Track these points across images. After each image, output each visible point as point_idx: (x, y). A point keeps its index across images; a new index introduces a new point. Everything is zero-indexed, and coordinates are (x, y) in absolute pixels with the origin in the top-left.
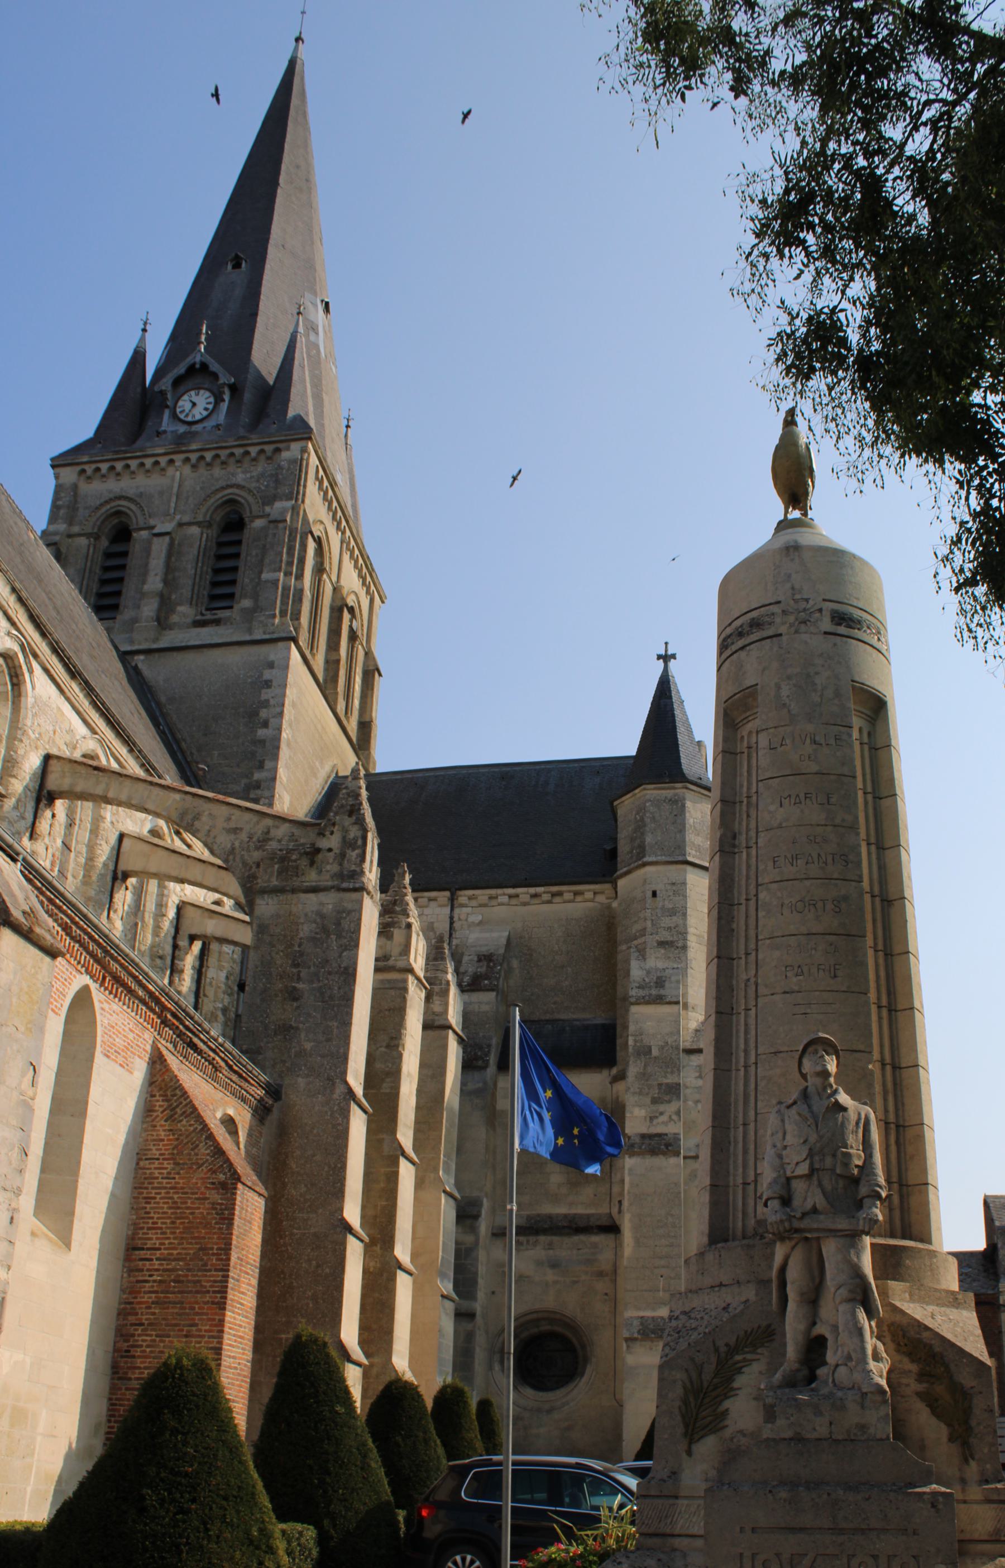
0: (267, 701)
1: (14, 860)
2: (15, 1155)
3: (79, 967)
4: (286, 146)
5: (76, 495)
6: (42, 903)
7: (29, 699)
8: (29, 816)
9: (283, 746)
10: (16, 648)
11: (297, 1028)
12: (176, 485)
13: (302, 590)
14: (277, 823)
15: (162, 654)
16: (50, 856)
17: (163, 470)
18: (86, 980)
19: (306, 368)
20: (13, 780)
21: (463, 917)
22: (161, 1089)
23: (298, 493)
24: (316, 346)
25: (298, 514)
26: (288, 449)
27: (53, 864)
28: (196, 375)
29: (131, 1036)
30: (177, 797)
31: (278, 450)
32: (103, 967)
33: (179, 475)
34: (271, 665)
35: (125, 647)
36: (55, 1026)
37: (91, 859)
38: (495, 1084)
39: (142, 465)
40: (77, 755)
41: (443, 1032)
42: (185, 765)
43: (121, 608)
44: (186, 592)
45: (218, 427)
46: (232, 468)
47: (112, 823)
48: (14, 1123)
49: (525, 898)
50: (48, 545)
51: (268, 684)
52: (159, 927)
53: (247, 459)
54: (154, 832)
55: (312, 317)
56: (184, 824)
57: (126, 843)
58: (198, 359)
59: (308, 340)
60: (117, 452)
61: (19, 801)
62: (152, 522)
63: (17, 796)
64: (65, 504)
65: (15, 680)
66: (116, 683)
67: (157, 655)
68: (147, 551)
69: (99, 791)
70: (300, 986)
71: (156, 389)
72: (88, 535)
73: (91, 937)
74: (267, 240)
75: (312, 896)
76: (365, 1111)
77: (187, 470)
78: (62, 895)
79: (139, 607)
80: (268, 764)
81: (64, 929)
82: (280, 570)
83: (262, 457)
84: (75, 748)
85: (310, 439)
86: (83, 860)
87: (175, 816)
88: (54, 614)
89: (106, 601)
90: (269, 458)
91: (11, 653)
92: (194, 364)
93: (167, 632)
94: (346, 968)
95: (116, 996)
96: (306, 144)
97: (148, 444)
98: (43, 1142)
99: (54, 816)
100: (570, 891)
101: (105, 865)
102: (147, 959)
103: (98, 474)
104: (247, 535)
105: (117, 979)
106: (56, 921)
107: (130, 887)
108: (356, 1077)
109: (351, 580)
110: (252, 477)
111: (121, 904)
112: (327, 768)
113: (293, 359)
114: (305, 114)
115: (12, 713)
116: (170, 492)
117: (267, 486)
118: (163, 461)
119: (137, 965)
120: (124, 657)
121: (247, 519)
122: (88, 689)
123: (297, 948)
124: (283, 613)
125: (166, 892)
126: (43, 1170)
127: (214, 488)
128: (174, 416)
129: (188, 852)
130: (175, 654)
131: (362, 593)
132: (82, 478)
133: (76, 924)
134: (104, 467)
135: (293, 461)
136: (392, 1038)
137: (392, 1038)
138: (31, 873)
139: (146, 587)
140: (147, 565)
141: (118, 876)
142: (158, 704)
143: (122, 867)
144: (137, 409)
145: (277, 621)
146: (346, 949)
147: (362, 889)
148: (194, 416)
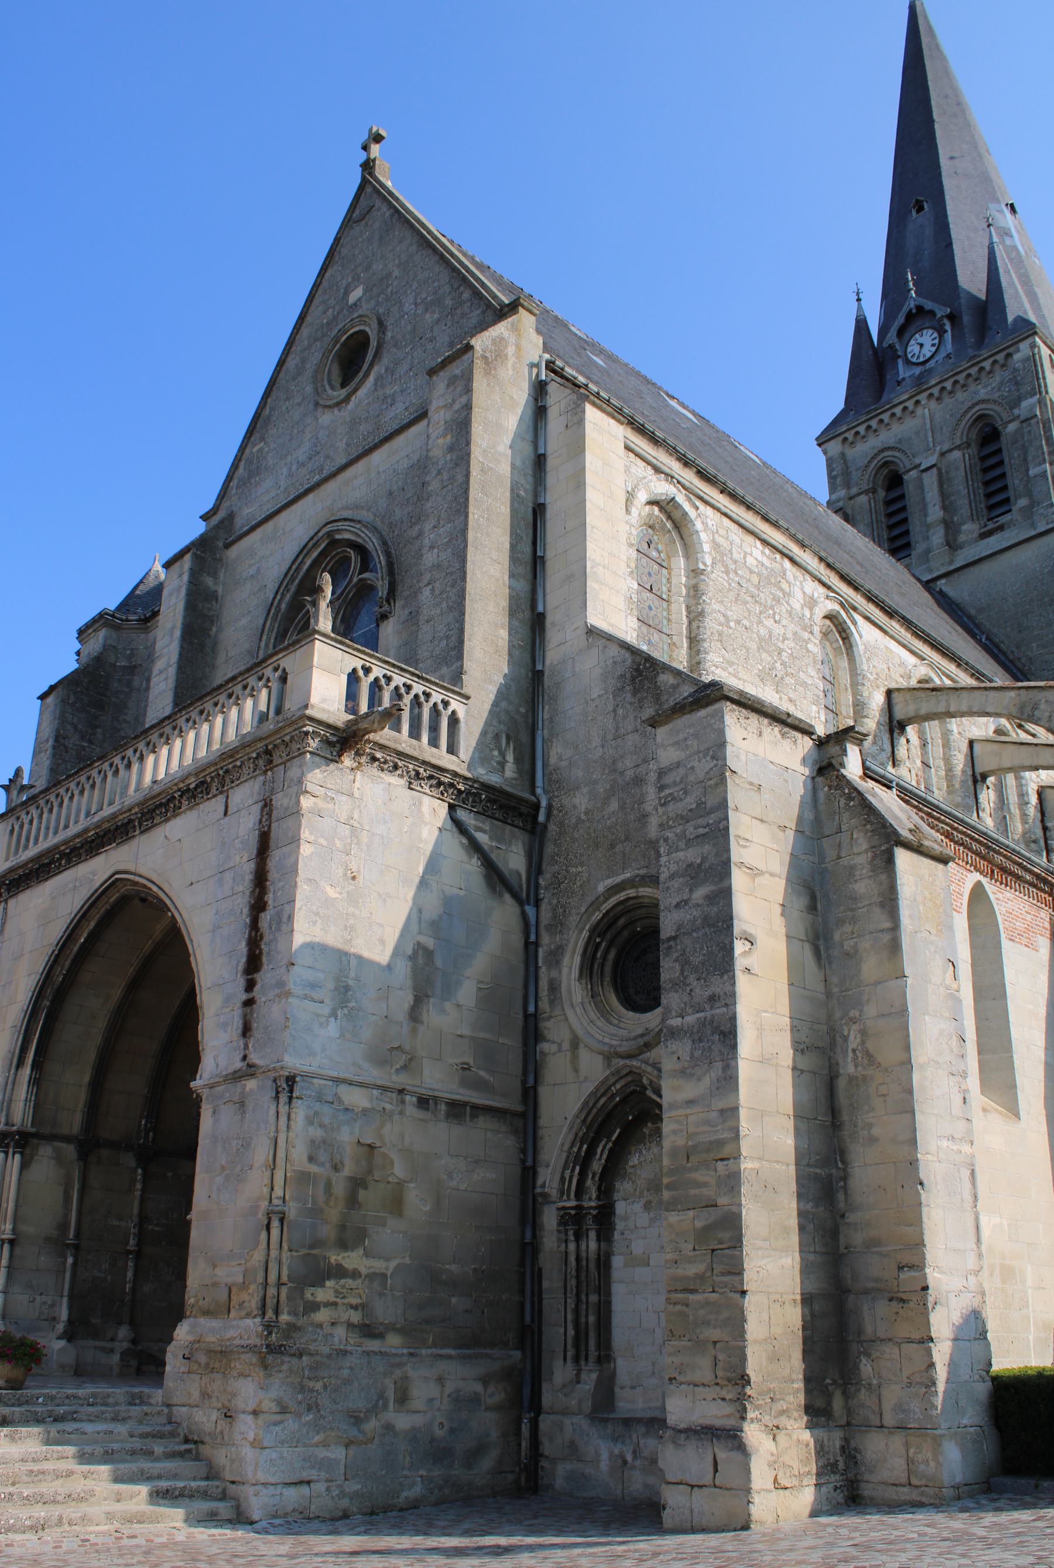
1: (889, 788)
2: (954, 1043)
3: (968, 867)
4: (930, 83)
5: (845, 462)
6: (922, 818)
7: (860, 646)
8: (887, 746)
10: (837, 607)
12: (928, 421)
15: (960, 573)
16: (914, 776)
17: (913, 412)
18: (977, 876)
19: (1012, 272)
20: (866, 720)
23: (1039, 386)
24: (1014, 248)
25: (1046, 405)
26: (1018, 350)
27: (918, 782)
28: (917, 318)
29: (1029, 918)
30: (1013, 694)
32: (990, 862)
33: (929, 411)
35: (926, 578)
36: (961, 923)
37: (949, 770)
39: (893, 415)
40: (913, 683)
42: (1009, 664)
43: (913, 544)
44: (965, 511)
45: (948, 356)
46: (972, 388)
47: (960, 733)
48: (947, 1015)
50: (836, 512)
52: (1026, 815)
53: (983, 374)
54: (999, 731)
55: (1002, 224)
56: (1025, 716)
57: (977, 747)
58: (912, 304)
59: (1005, 246)
60: (868, 413)
61: (875, 736)
62: (917, 461)
63: (873, 733)
64: (839, 474)
65: (844, 635)
66: (929, 610)
67: (956, 575)
68: (921, 487)
69: (941, 708)
71: (885, 345)
72: (866, 492)
73: (972, 838)
74: (940, 174)
77: (933, 404)
78: (937, 807)
79: (928, 538)
81: (946, 837)
82: (1044, 461)
83: (997, 367)
84: (910, 677)
85: (1035, 333)
86: (944, 773)
87: (1014, 711)
88: (858, 568)
89: (898, 543)
90: (1003, 366)
91: (834, 613)
92: (911, 310)
93: (959, 552)
95: (1006, 885)
96: (946, 72)
97: (893, 395)
98: (974, 1027)
99: (908, 741)
101: (963, 772)
102: (1022, 846)
103: (859, 438)
105: (1003, 870)
106: (938, 831)
107: (990, 786)
110: (993, 389)
111: (986, 803)
113: (997, 269)
114: (937, 47)
115: (849, 664)
116: (925, 430)
117: (1009, 391)
118: (910, 404)
119: (1018, 853)
120: (928, 585)
121: (1000, 428)
122: (907, 623)
125: (1023, 782)
126: (979, 1053)
127: (962, 411)
128: (908, 363)
129: (1035, 741)
130: (972, 569)
132: (846, 445)
133: (956, 829)
134: (862, 429)
135: (1026, 360)
138: (907, 795)
139: (929, 519)
140: (924, 499)
141: (978, 779)
142: (969, 617)
143: (979, 770)
144: (874, 369)
148: (924, 356)
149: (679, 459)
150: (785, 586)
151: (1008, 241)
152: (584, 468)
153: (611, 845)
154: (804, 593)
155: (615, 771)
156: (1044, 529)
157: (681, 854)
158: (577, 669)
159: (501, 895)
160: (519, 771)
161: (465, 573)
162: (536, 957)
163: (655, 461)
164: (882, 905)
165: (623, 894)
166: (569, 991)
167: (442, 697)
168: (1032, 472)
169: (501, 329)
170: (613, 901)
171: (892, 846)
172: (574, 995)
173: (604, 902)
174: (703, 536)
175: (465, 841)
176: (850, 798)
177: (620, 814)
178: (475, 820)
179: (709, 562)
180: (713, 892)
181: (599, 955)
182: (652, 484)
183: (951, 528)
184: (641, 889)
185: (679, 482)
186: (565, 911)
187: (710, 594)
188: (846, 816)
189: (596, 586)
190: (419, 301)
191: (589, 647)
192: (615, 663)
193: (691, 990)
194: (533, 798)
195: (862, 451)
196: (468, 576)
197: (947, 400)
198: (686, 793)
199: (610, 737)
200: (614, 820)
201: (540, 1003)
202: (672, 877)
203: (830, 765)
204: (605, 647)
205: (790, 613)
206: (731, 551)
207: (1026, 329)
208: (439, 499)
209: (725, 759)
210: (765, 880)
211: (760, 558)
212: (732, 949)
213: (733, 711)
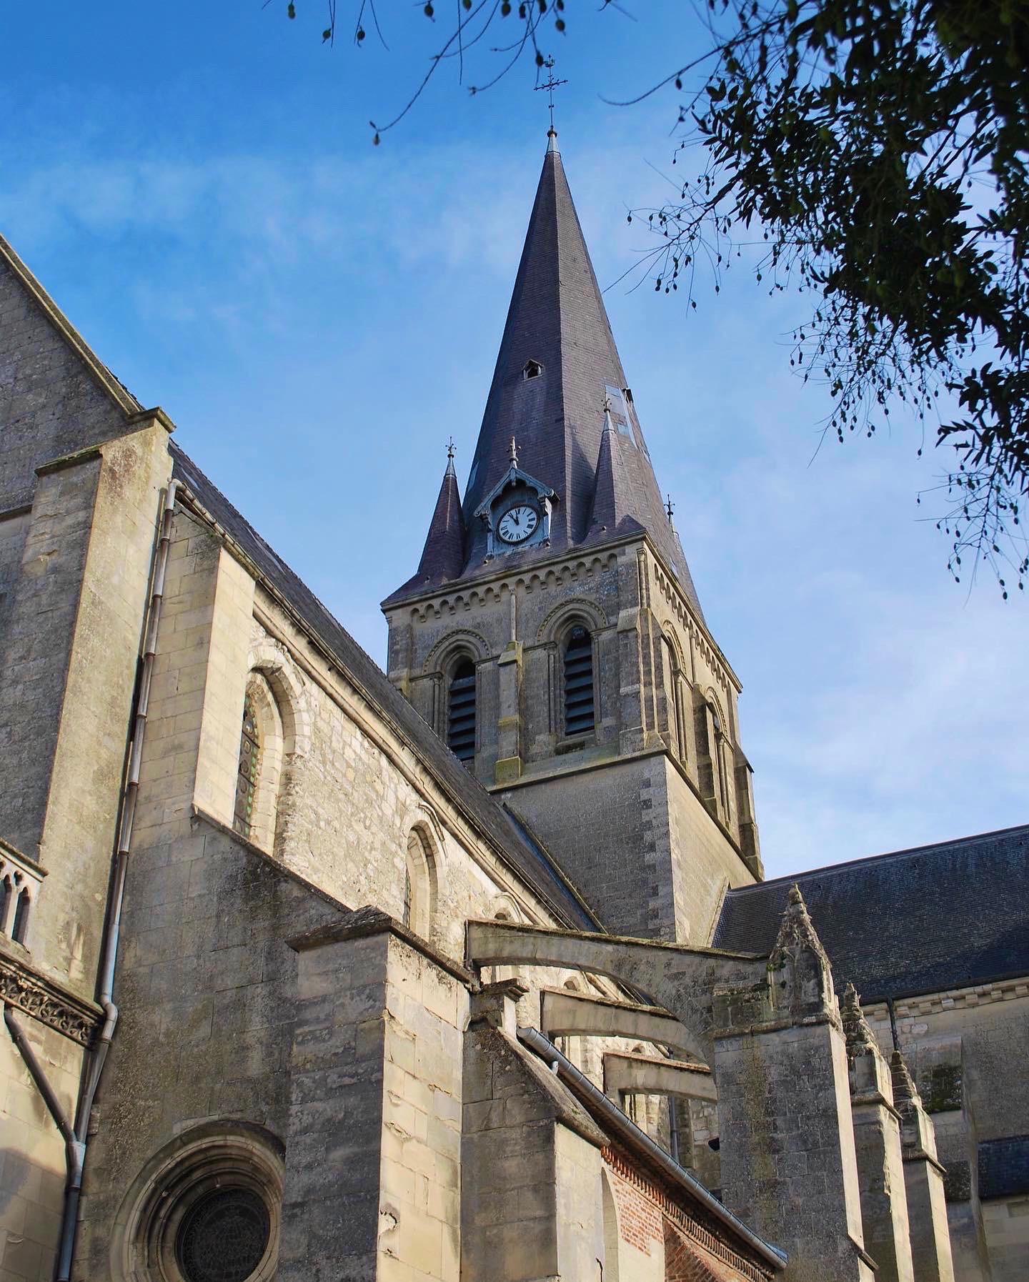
0: (650, 822)
5: (412, 637)
9: (675, 868)
10: (427, 819)
11: (784, 1183)
13: (664, 699)
14: (720, 962)
15: (530, 789)
21: (906, 1029)
22: (679, 1269)
28: (517, 493)
29: (644, 1215)
31: (613, 556)
34: (647, 784)
38: (981, 1218)
40: (491, 917)
41: (919, 1165)
43: (477, 746)
46: (568, 583)
49: (972, 999)
51: (647, 804)
58: (513, 477)
62: (495, 653)
67: (524, 790)
68: (496, 684)
70: (779, 1136)
75: (773, 1036)
76: (872, 1268)
77: (522, 591)
80: (662, 891)
90: (604, 566)
92: (510, 482)
94: (825, 1111)
100: (1022, 985)
104: (596, 649)
108: (856, 1232)
109: (706, 677)
112: (719, 883)
123: (767, 1095)
124: (651, 726)
127: (553, 607)
128: (498, 539)
130: (543, 786)
131: (718, 687)
132: (416, 617)
135: (631, 565)
136: (874, 1181)
137: (874, 1181)
140: (498, 697)
144: (458, 538)
145: (645, 735)
146: (821, 1090)
147: (824, 1021)
148: (518, 535)
149: (293, 625)
150: (379, 787)
151: (621, 429)
152: (210, 624)
153: (197, 1077)
154: (397, 798)
155: (211, 988)
156: (629, 756)
157: (319, 1105)
158: (174, 859)
159: (47, 1125)
160: (86, 972)
161: (58, 722)
162: (78, 1208)
163: (268, 623)
164: (535, 1190)
165: (207, 1140)
166: (120, 1258)
167: (15, 869)
168: (623, 690)
169: (133, 440)
170: (192, 1147)
171: (552, 1122)
172: (125, 1261)
173: (180, 1148)
174: (305, 716)
175: (17, 1052)
176: (505, 1061)
177: (212, 1042)
178: (32, 1025)
179: (307, 748)
180: (356, 1155)
181: (162, 1213)
182: (261, 648)
183: (525, 735)
184: (231, 1138)
185: (289, 651)
186: (124, 1153)
187: (304, 786)
188: (500, 1081)
189: (207, 764)
190: (20, 376)
191: (193, 835)
192: (225, 860)
193: (318, 1270)
194: (97, 1007)
195: (437, 626)
196: (62, 726)
197: (538, 591)
198: (331, 1034)
199: (208, 947)
200: (204, 1048)
201: (75, 1269)
202: (305, 1131)
203: (484, 1020)
204: (214, 839)
205: (381, 818)
206: (330, 738)
207: (634, 533)
208: (33, 625)
209: (384, 1001)
210: (412, 1146)
211: (358, 750)
212: (375, 1225)
213: (396, 946)
